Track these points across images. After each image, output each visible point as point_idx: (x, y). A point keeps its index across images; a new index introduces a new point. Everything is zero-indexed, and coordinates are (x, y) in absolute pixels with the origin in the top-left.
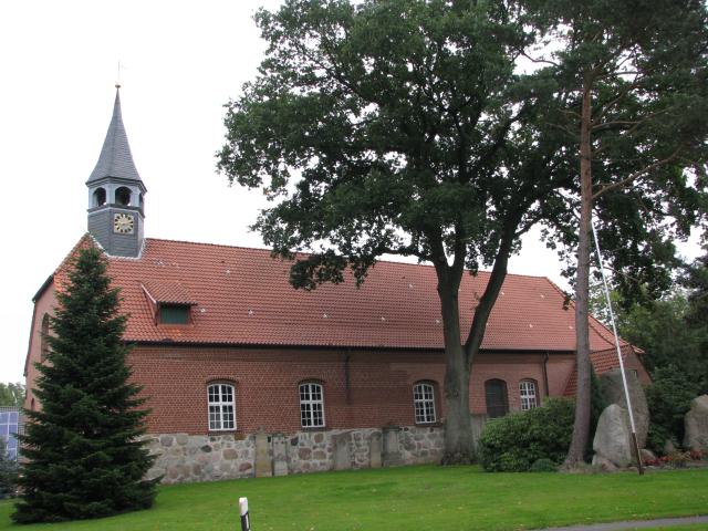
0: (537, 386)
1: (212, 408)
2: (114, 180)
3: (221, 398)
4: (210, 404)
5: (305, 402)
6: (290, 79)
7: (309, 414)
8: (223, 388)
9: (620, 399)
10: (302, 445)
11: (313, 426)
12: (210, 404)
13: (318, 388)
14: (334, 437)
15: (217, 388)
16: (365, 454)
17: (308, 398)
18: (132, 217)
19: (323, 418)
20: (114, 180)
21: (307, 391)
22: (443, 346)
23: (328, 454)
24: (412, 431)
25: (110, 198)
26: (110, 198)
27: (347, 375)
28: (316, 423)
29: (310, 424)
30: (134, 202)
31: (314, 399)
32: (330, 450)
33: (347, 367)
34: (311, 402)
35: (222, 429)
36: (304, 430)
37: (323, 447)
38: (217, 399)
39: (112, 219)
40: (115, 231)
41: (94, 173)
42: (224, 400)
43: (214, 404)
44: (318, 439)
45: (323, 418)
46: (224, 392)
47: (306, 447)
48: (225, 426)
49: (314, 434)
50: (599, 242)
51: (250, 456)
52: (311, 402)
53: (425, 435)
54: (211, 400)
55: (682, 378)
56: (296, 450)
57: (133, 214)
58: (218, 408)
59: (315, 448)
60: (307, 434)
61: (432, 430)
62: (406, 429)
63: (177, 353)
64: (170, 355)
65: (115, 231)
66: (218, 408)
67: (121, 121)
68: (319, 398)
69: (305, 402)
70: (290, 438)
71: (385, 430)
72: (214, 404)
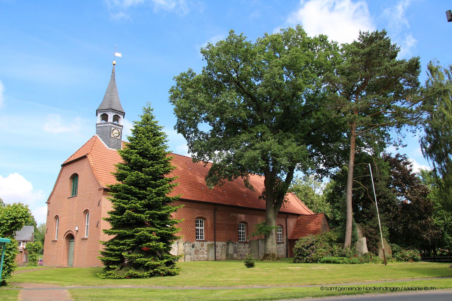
0: (283, 229)
2: (114, 110)
5: (197, 228)
6: (307, 172)
9: (272, 234)
11: (200, 239)
13: (202, 221)
14: (208, 245)
15: (198, 220)
16: (220, 253)
18: (119, 130)
19: (204, 236)
20: (114, 110)
22: (265, 209)
23: (206, 253)
24: (238, 245)
25: (110, 119)
26: (110, 119)
27: (214, 216)
28: (201, 238)
29: (198, 238)
32: (206, 251)
33: (214, 213)
34: (199, 228)
36: (197, 241)
37: (204, 249)
39: (111, 130)
40: (112, 136)
44: (202, 245)
45: (204, 236)
49: (201, 243)
50: (380, 232)
51: (175, 251)
52: (199, 228)
53: (242, 247)
57: (120, 129)
59: (200, 249)
60: (198, 243)
61: (244, 245)
62: (235, 244)
65: (112, 136)
68: (202, 227)
69: (197, 228)
70: (192, 244)
71: (228, 244)
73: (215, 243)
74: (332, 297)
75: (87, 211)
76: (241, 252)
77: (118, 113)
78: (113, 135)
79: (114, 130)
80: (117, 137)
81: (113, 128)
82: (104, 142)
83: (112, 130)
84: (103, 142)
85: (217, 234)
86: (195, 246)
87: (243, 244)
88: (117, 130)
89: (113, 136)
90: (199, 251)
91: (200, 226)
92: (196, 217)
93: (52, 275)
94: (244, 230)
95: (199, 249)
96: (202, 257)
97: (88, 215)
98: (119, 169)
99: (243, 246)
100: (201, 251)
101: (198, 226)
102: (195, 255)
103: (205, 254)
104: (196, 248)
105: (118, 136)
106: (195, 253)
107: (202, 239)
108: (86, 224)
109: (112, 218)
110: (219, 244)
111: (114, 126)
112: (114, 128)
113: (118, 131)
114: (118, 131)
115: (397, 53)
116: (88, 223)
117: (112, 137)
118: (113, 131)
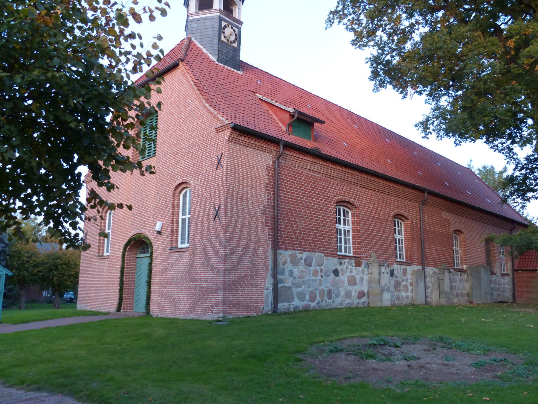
28: (346, 252)
32: (411, 284)
37: (407, 280)
57: (237, 27)
60: (399, 266)
61: (461, 275)
73: (423, 269)
74: (25, 325)
75: (184, 185)
76: (458, 289)
79: (225, 26)
81: (224, 24)
82: (207, 50)
83: (223, 26)
84: (204, 50)
86: (396, 272)
87: (459, 273)
91: (345, 224)
92: (393, 213)
93: (498, 362)
94: (348, 225)
95: (401, 280)
96: (405, 296)
97: (185, 196)
99: (459, 277)
101: (340, 223)
103: (410, 290)
104: (396, 277)
105: (234, 42)
106: (395, 287)
107: (458, 268)
108: (181, 217)
110: (429, 270)
113: (234, 30)
116: (184, 214)
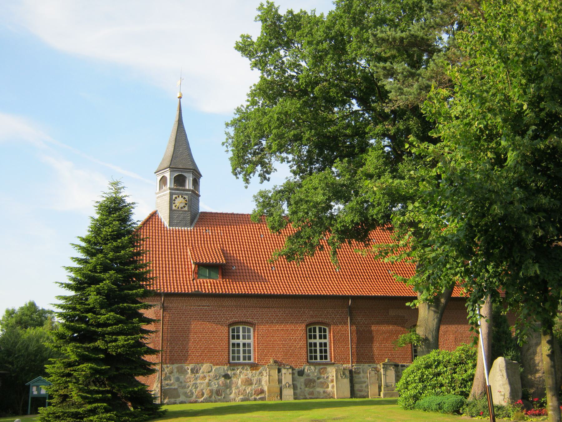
1: (234, 345)
3: (241, 337)
4: (232, 341)
5: (313, 341)
7: (315, 351)
8: (320, 329)
10: (308, 375)
12: (232, 341)
15: (315, 329)
17: (315, 337)
21: (315, 331)
29: (316, 358)
30: (189, 185)
31: (320, 338)
35: (242, 361)
36: (315, 364)
38: (315, 338)
41: (161, 163)
42: (320, 338)
43: (236, 341)
46: (320, 331)
47: (311, 378)
48: (244, 358)
54: (233, 338)
55: (211, 218)
56: (302, 379)
57: (187, 194)
58: (238, 345)
60: (312, 367)
63: (206, 302)
64: (200, 303)
66: (238, 345)
67: (183, 127)
69: (313, 341)
72: (236, 341)
77: (181, 171)
78: (175, 206)
79: (176, 198)
80: (182, 208)
85: (443, 328)
88: (182, 197)
89: (176, 208)
90: (315, 381)
98: (276, 104)
100: (319, 381)
102: (307, 389)
106: (306, 385)
109: (355, 131)
111: (176, 192)
112: (177, 196)
113: (184, 198)
114: (184, 198)
115: (374, 228)
117: (175, 210)
118: (174, 200)
